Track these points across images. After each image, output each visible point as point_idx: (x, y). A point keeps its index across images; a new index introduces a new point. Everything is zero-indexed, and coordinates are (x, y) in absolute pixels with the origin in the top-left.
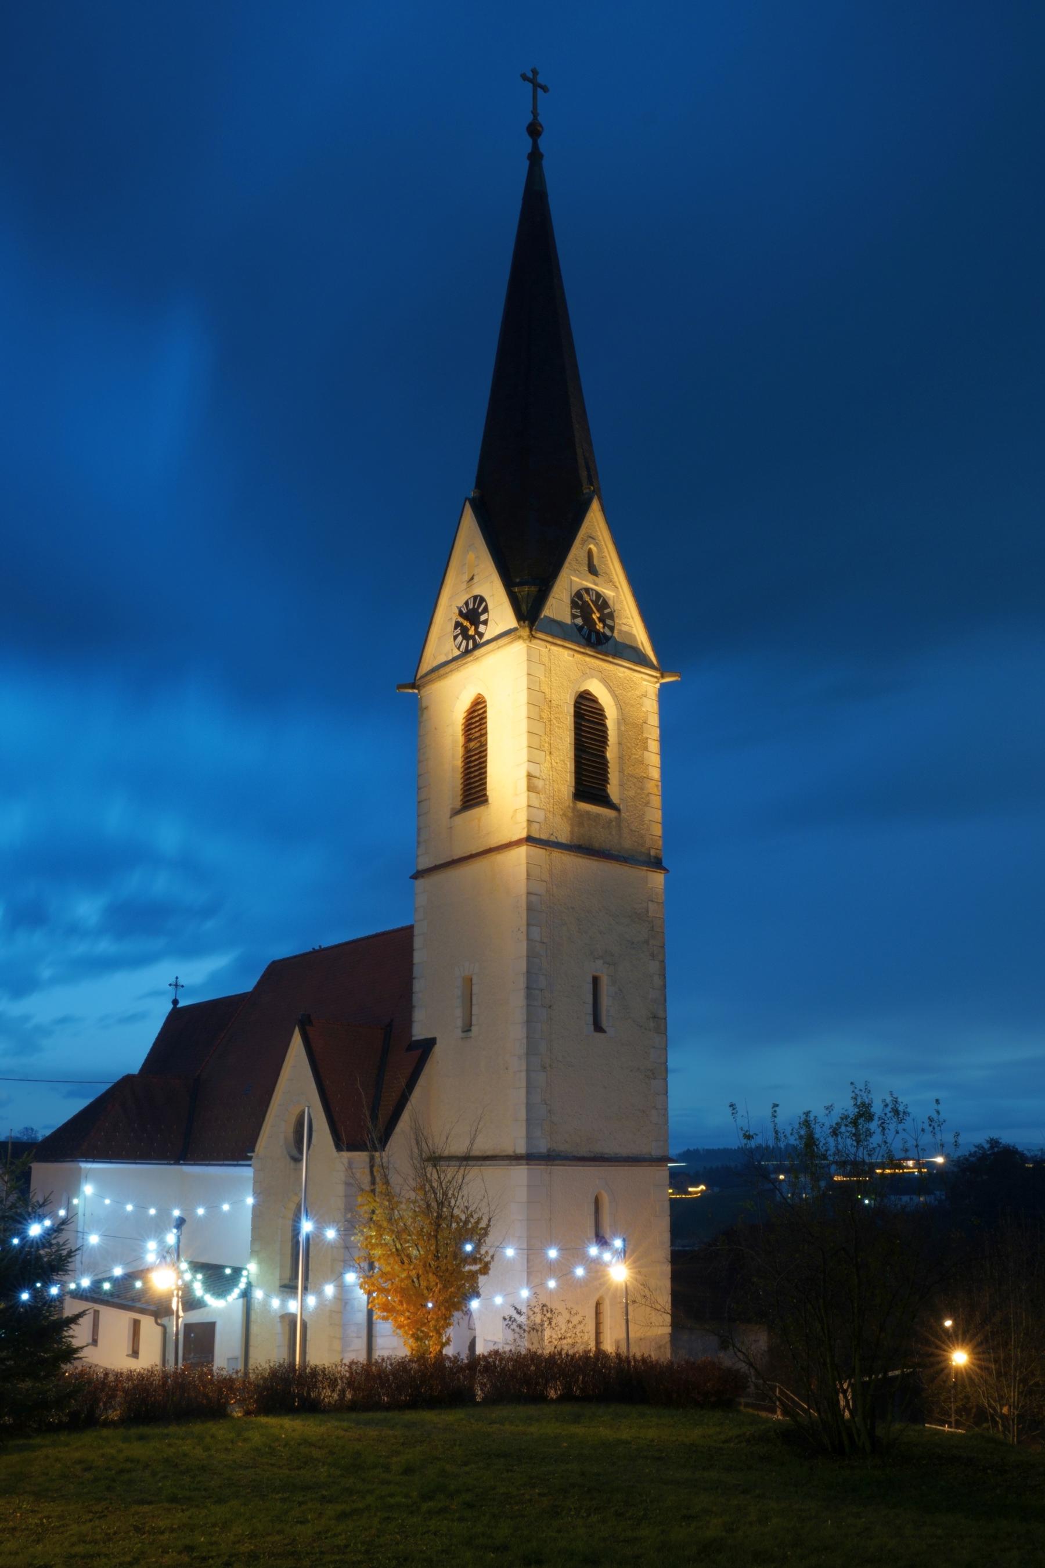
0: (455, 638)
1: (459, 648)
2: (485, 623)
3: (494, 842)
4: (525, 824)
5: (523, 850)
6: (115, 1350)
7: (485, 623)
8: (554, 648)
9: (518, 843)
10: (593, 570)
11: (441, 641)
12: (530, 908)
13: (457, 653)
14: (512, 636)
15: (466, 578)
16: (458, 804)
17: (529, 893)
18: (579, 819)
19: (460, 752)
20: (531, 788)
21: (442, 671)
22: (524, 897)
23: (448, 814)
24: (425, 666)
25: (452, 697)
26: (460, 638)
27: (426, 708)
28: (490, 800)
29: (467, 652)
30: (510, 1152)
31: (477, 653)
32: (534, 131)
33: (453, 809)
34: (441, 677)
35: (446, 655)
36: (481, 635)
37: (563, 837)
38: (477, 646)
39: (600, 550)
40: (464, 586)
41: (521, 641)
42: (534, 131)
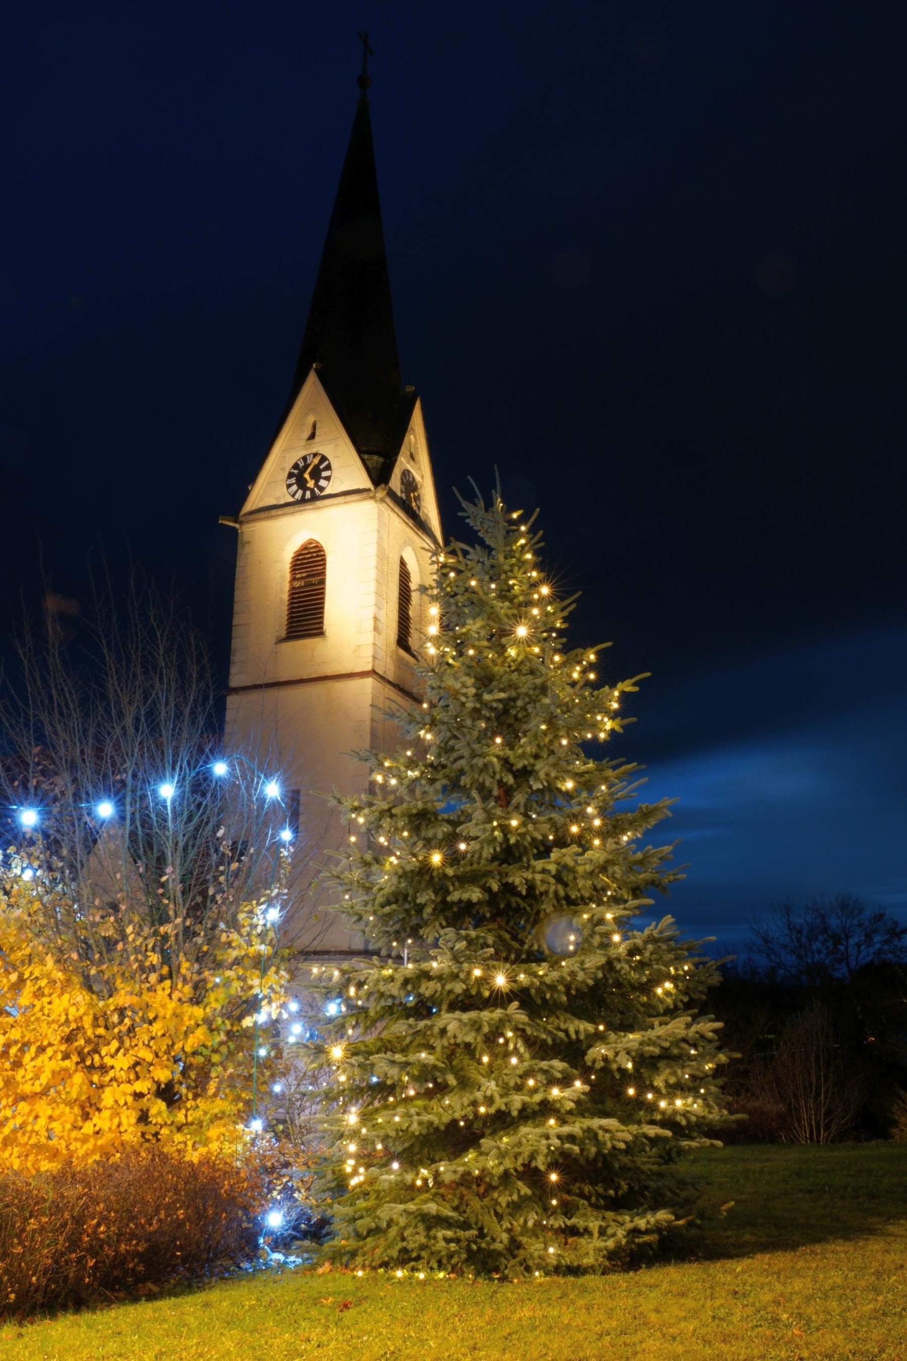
0: (289, 486)
1: (293, 496)
2: (328, 479)
3: (330, 671)
4: (370, 659)
5: (369, 682)
6: (722, 979)
7: (328, 479)
8: (392, 514)
9: (363, 674)
10: (412, 457)
11: (271, 483)
12: (373, 734)
13: (291, 499)
14: (364, 495)
15: (308, 433)
16: (283, 634)
17: (372, 720)
18: (400, 664)
19: (287, 587)
20: (376, 629)
21: (273, 512)
22: (368, 723)
23: (273, 641)
24: (249, 506)
25: (276, 541)
26: (295, 487)
27: (249, 543)
28: (328, 633)
29: (303, 501)
30: (345, 947)
31: (319, 503)
32: (363, 82)
33: (277, 637)
34: (268, 518)
35: (277, 499)
36: (322, 489)
37: (390, 677)
38: (315, 498)
39: (416, 443)
40: (303, 442)
41: (372, 501)
42: (363, 82)
